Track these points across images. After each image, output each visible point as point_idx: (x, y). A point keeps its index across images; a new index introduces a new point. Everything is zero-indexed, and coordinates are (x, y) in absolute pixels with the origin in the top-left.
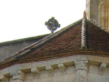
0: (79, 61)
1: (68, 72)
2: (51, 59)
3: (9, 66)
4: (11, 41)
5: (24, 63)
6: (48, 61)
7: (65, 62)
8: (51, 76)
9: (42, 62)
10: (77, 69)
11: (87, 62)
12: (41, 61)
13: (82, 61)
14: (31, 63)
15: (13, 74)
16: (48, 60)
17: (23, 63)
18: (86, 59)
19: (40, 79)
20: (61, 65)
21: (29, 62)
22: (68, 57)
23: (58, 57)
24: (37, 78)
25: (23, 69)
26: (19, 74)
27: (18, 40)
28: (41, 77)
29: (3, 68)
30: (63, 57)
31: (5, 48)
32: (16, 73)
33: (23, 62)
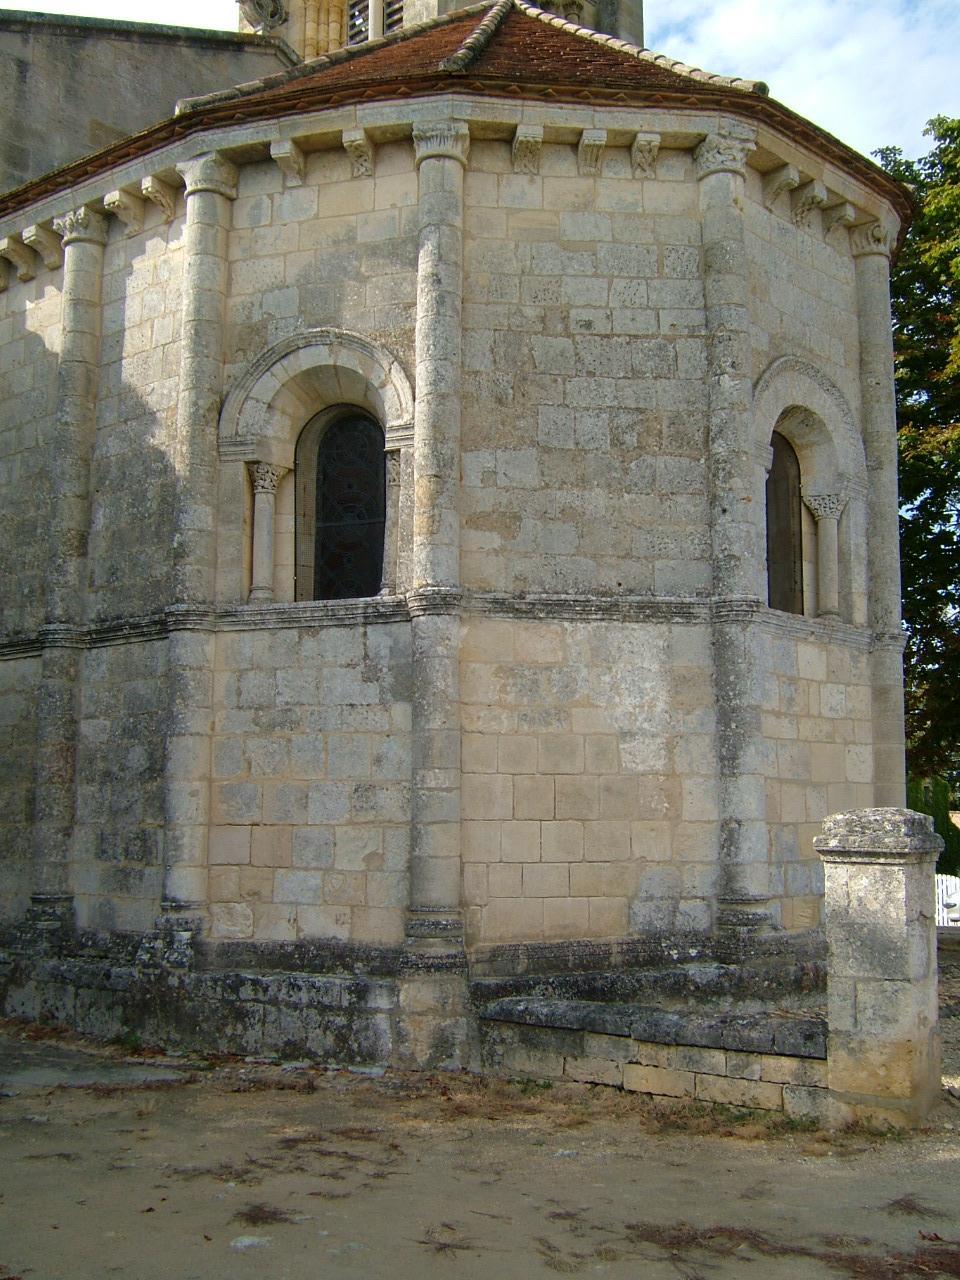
0: (724, 137)
1: (662, 172)
2: (611, 102)
3: (406, 95)
4: (140, 24)
5: (490, 96)
6: (598, 108)
7: (669, 130)
8: (587, 175)
9: (570, 106)
10: (419, 155)
11: (753, 147)
12: (568, 102)
13: (736, 138)
14: (519, 102)
15: (428, 135)
16: (600, 105)
17: (482, 95)
18: (752, 136)
19: (538, 179)
20: (649, 137)
21: (513, 95)
22: (687, 112)
23: (647, 104)
24: (525, 170)
25: (480, 119)
26: (458, 138)
27: (162, 26)
28: (543, 172)
29: (371, 99)
30: (666, 108)
31: (116, 43)
32: (446, 133)
33: (486, 92)
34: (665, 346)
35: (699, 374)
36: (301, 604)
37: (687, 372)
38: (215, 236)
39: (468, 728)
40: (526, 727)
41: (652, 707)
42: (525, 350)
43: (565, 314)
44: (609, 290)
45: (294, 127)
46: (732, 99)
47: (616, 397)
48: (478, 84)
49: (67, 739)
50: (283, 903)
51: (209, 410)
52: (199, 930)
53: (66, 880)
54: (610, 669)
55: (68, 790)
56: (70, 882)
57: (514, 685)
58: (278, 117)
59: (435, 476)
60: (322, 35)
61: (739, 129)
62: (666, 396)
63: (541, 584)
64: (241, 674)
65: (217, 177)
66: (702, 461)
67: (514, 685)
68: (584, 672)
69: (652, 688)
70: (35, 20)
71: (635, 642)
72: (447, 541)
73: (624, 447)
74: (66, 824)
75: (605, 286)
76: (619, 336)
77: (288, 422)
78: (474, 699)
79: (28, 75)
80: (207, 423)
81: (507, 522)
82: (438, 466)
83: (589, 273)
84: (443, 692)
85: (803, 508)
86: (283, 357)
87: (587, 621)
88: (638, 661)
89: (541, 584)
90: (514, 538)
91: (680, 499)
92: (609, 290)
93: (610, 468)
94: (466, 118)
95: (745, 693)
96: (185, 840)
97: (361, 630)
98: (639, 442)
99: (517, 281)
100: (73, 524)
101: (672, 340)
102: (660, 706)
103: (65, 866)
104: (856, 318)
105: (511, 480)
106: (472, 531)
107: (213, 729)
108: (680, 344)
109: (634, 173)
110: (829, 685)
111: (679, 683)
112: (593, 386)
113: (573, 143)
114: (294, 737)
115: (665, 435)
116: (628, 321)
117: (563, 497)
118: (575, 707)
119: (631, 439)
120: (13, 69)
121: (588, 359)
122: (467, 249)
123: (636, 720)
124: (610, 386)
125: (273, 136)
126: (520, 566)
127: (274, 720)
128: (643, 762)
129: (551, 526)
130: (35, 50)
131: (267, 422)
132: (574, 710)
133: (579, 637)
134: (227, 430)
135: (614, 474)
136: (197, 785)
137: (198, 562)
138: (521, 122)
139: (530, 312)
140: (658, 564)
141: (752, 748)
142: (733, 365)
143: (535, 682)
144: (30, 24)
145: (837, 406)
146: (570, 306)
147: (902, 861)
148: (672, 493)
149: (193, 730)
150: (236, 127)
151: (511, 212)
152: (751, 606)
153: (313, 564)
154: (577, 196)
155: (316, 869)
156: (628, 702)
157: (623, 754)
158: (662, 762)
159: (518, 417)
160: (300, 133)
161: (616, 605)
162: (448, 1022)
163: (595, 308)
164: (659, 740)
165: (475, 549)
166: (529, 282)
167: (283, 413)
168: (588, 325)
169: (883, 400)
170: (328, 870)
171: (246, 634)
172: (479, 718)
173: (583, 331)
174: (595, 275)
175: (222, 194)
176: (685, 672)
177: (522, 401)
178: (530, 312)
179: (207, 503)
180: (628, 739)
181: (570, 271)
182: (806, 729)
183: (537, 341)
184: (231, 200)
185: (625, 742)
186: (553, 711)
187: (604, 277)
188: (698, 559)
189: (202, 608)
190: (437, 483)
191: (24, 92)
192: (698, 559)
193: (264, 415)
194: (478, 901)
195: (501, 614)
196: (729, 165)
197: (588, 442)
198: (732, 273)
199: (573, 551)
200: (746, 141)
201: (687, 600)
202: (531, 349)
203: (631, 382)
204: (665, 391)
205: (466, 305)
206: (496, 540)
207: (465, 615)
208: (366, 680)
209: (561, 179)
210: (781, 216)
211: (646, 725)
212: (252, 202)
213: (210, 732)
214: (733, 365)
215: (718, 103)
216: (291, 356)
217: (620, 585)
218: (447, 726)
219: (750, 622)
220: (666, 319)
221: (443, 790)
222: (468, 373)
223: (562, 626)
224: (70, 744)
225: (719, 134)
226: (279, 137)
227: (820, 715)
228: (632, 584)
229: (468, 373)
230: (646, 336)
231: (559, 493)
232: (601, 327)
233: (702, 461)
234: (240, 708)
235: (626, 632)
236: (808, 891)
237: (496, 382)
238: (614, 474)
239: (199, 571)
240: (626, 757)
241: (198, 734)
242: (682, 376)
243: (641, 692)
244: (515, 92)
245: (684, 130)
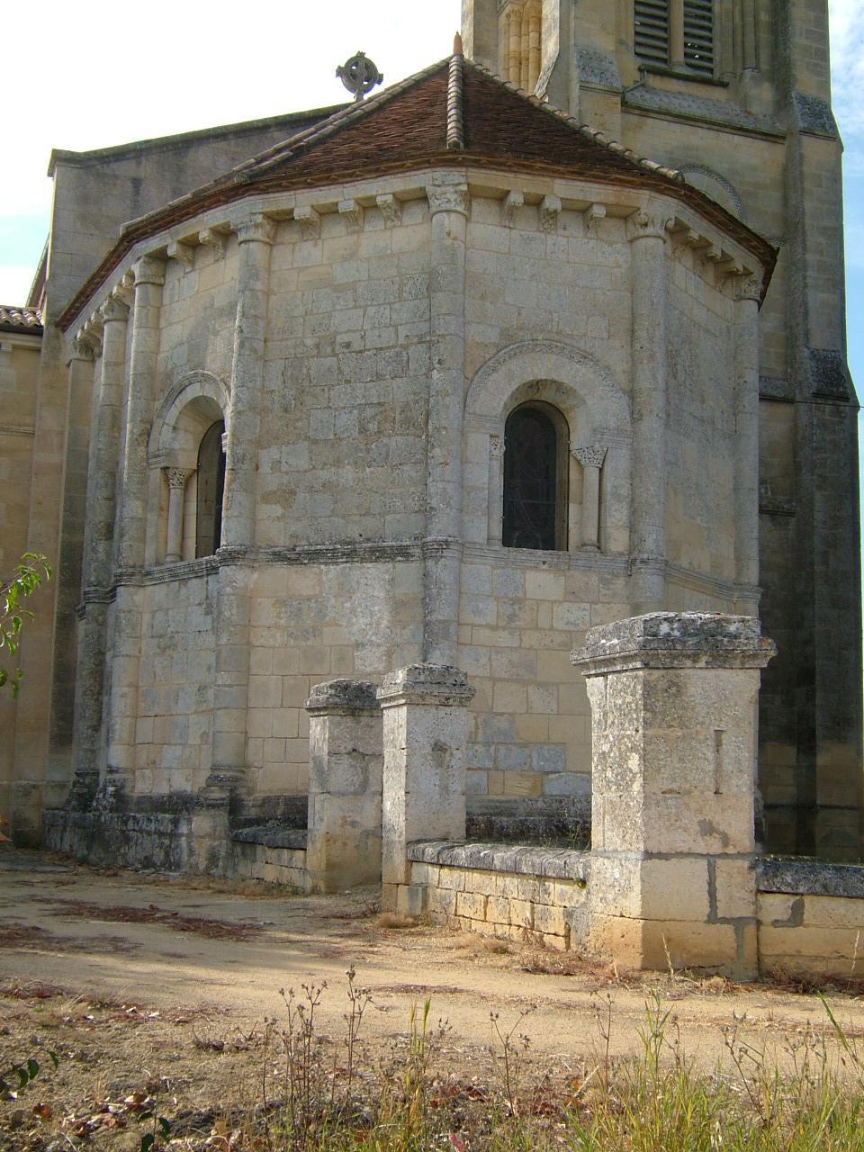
1: (407, 219)
2: (353, 179)
3: (226, 202)
4: (233, 125)
5: (274, 192)
6: (345, 185)
7: (398, 190)
9: (326, 188)
13: (449, 185)
14: (292, 192)
16: (347, 183)
17: (268, 193)
19: (320, 242)
20: (384, 198)
21: (287, 189)
22: (408, 174)
23: (378, 174)
24: (311, 238)
26: (257, 226)
28: (323, 236)
29: (209, 208)
30: (392, 174)
31: (214, 145)
33: (270, 190)
34: (401, 352)
35: (424, 370)
36: (200, 560)
37: (415, 370)
38: (147, 314)
39: (255, 643)
40: (292, 642)
41: (378, 624)
42: (305, 371)
43: (333, 340)
44: (364, 316)
45: (177, 233)
46: (439, 157)
47: (364, 397)
48: (261, 187)
49: (97, 665)
50: (164, 768)
51: (140, 435)
52: (123, 787)
53: (94, 761)
54: (351, 597)
55: (97, 700)
56: (97, 762)
57: (286, 612)
58: (169, 228)
59: (232, 469)
60: (524, 45)
61: (451, 177)
62: (399, 391)
63: (308, 539)
64: (154, 613)
65: (149, 272)
66: (424, 437)
67: (286, 612)
68: (333, 601)
69: (380, 611)
70: (144, 147)
71: (369, 577)
72: (236, 514)
73: (368, 433)
74: (95, 723)
75: (362, 314)
76: (369, 350)
77: (190, 437)
78: (259, 623)
79: (141, 188)
80: (139, 444)
81: (286, 496)
82: (234, 462)
83: (350, 306)
84: (229, 619)
85: (571, 458)
86: (180, 393)
87: (337, 563)
88: (370, 591)
89: (308, 539)
90: (291, 507)
91: (406, 468)
92: (364, 316)
93: (357, 449)
94: (261, 211)
95: (434, 611)
96: (117, 727)
97: (206, 579)
98: (378, 428)
99: (302, 320)
100: (102, 518)
101: (405, 347)
102: (385, 623)
103: (93, 751)
104: (629, 295)
105: (290, 466)
106: (264, 505)
107: (140, 652)
108: (412, 349)
109: (385, 224)
110: (565, 603)
111: (398, 605)
112: (349, 391)
113: (329, 212)
114: (175, 656)
115: (397, 421)
116: (376, 338)
117: (324, 475)
118: (326, 626)
119: (373, 427)
120: (129, 187)
121: (346, 370)
122: (271, 303)
123: (367, 634)
124: (360, 389)
125: (169, 241)
126: (295, 528)
127: (167, 643)
128: (371, 665)
129: (317, 497)
130: (147, 169)
131: (173, 439)
132: (325, 629)
133: (330, 576)
134: (152, 448)
135: (360, 455)
136: (125, 690)
137: (130, 539)
138: (296, 206)
139: (309, 342)
140: (388, 518)
141: (438, 652)
142: (440, 362)
143: (300, 610)
144: (141, 150)
145: (595, 372)
146: (337, 333)
147: (326, 713)
148: (400, 464)
149: (124, 653)
150: (151, 238)
151: (301, 270)
152: (441, 545)
153: (213, 535)
154: (346, 249)
155: (180, 744)
156: (362, 622)
157: (356, 659)
158: (383, 665)
159: (297, 420)
160: (181, 237)
161: (355, 551)
162: (216, 843)
163: (354, 331)
164: (382, 649)
165: (265, 517)
166: (310, 319)
167: (186, 431)
168: (348, 345)
169: (645, 361)
170: (184, 745)
171: (157, 587)
172: (262, 636)
173: (345, 350)
174: (355, 307)
175: (153, 284)
176: (404, 598)
177: (300, 407)
178: (309, 342)
179: (138, 499)
180: (360, 648)
181: (338, 307)
182: (531, 639)
183: (314, 362)
184: (161, 286)
185: (358, 651)
186: (311, 630)
187: (360, 307)
188: (417, 512)
189: (130, 570)
190: (232, 474)
191: (138, 201)
192: (417, 512)
193: (171, 435)
194: (256, 764)
195: (279, 563)
196: (444, 207)
197: (343, 432)
198: (442, 291)
199: (329, 514)
200: (460, 184)
201: (405, 544)
202: (309, 369)
203: (377, 384)
204: (399, 387)
205: (268, 344)
206: (278, 510)
207: (256, 565)
208: (207, 614)
209: (336, 238)
210: (526, 228)
211: (374, 638)
212: (171, 284)
213: (138, 654)
214: (440, 362)
215: (428, 162)
216: (183, 393)
217: (361, 535)
218: (231, 641)
219: (442, 557)
220: (403, 332)
221: (225, 686)
222: (267, 393)
223: (320, 568)
224: (99, 668)
225: (435, 185)
226: (168, 240)
227: (552, 628)
228: (370, 534)
229: (267, 393)
230: (388, 348)
231: (321, 472)
232: (357, 346)
233: (424, 437)
234: (152, 637)
235: (363, 570)
236: (526, 768)
237: (284, 397)
238: (360, 455)
239: (130, 545)
240: (358, 662)
241: (127, 655)
242: (412, 373)
243: (372, 614)
244: (288, 187)
245: (407, 188)
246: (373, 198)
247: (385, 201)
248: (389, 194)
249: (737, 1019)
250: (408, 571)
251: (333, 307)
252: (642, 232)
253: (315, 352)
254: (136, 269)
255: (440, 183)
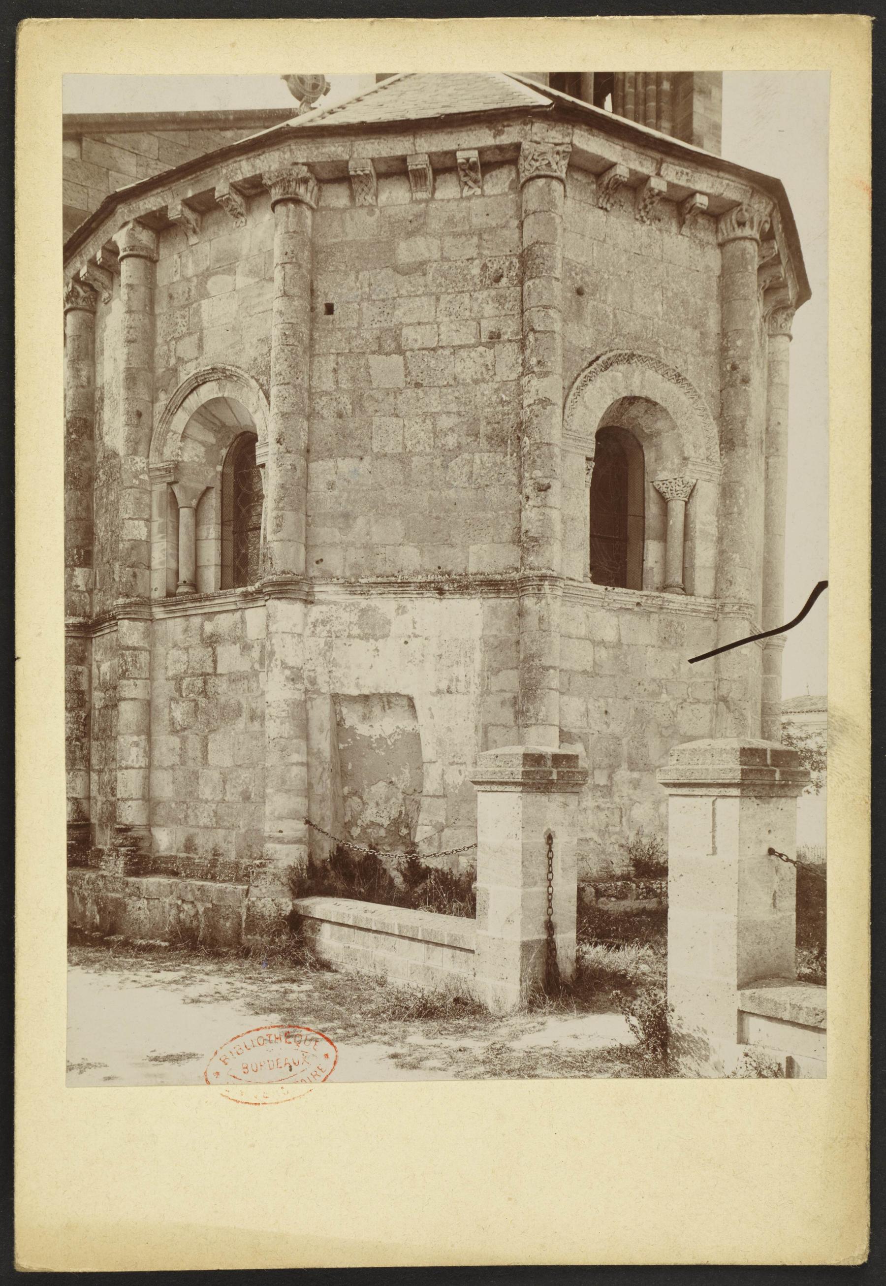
20: (466, 154)
246: (453, 153)
247: (468, 160)
248: (475, 149)
249: (241, 944)
250: (505, 603)
251: (398, 291)
252: (739, 232)
253: (375, 347)
254: (121, 239)
255: (538, 139)
